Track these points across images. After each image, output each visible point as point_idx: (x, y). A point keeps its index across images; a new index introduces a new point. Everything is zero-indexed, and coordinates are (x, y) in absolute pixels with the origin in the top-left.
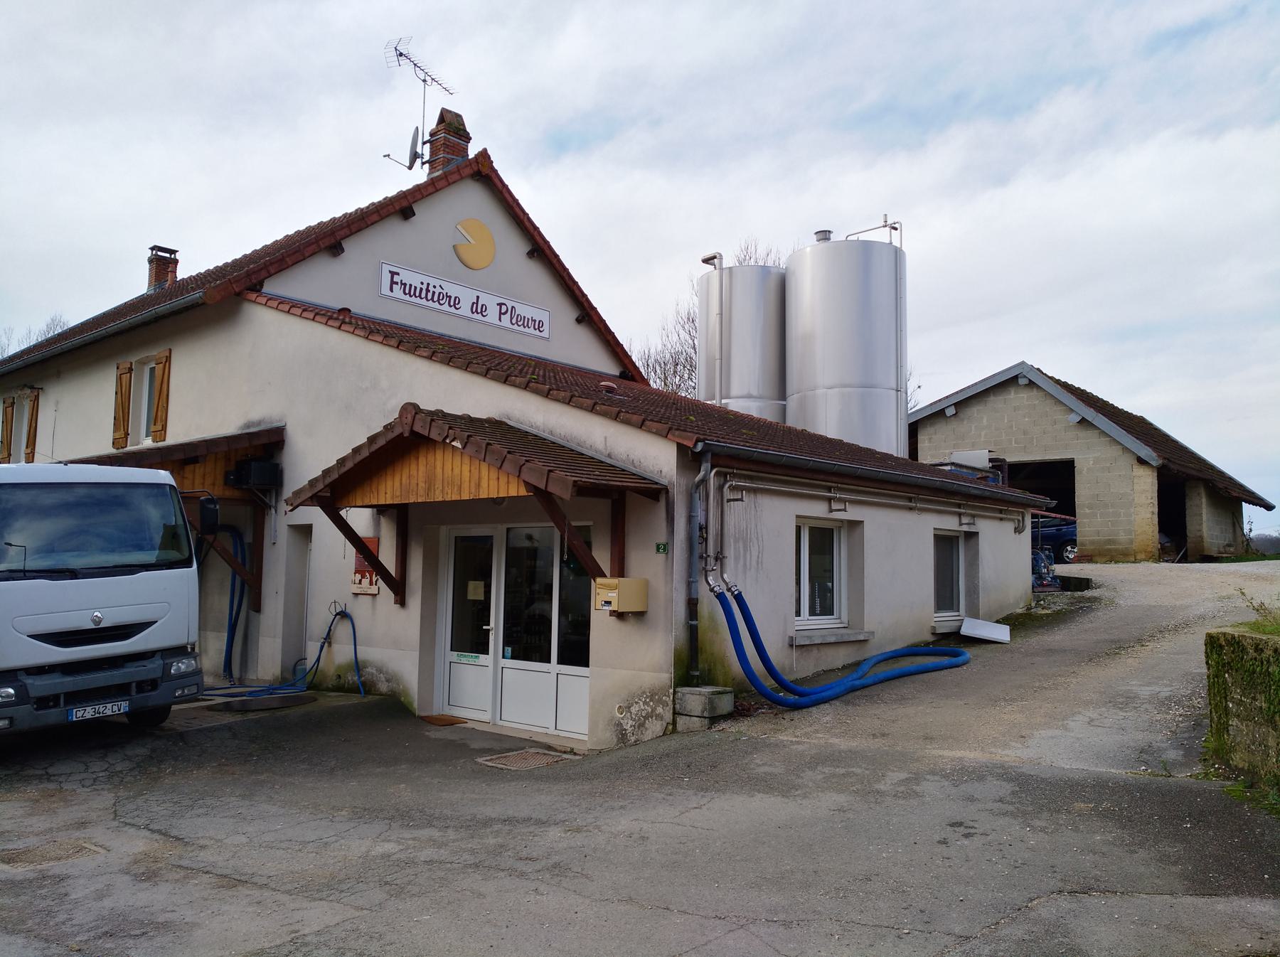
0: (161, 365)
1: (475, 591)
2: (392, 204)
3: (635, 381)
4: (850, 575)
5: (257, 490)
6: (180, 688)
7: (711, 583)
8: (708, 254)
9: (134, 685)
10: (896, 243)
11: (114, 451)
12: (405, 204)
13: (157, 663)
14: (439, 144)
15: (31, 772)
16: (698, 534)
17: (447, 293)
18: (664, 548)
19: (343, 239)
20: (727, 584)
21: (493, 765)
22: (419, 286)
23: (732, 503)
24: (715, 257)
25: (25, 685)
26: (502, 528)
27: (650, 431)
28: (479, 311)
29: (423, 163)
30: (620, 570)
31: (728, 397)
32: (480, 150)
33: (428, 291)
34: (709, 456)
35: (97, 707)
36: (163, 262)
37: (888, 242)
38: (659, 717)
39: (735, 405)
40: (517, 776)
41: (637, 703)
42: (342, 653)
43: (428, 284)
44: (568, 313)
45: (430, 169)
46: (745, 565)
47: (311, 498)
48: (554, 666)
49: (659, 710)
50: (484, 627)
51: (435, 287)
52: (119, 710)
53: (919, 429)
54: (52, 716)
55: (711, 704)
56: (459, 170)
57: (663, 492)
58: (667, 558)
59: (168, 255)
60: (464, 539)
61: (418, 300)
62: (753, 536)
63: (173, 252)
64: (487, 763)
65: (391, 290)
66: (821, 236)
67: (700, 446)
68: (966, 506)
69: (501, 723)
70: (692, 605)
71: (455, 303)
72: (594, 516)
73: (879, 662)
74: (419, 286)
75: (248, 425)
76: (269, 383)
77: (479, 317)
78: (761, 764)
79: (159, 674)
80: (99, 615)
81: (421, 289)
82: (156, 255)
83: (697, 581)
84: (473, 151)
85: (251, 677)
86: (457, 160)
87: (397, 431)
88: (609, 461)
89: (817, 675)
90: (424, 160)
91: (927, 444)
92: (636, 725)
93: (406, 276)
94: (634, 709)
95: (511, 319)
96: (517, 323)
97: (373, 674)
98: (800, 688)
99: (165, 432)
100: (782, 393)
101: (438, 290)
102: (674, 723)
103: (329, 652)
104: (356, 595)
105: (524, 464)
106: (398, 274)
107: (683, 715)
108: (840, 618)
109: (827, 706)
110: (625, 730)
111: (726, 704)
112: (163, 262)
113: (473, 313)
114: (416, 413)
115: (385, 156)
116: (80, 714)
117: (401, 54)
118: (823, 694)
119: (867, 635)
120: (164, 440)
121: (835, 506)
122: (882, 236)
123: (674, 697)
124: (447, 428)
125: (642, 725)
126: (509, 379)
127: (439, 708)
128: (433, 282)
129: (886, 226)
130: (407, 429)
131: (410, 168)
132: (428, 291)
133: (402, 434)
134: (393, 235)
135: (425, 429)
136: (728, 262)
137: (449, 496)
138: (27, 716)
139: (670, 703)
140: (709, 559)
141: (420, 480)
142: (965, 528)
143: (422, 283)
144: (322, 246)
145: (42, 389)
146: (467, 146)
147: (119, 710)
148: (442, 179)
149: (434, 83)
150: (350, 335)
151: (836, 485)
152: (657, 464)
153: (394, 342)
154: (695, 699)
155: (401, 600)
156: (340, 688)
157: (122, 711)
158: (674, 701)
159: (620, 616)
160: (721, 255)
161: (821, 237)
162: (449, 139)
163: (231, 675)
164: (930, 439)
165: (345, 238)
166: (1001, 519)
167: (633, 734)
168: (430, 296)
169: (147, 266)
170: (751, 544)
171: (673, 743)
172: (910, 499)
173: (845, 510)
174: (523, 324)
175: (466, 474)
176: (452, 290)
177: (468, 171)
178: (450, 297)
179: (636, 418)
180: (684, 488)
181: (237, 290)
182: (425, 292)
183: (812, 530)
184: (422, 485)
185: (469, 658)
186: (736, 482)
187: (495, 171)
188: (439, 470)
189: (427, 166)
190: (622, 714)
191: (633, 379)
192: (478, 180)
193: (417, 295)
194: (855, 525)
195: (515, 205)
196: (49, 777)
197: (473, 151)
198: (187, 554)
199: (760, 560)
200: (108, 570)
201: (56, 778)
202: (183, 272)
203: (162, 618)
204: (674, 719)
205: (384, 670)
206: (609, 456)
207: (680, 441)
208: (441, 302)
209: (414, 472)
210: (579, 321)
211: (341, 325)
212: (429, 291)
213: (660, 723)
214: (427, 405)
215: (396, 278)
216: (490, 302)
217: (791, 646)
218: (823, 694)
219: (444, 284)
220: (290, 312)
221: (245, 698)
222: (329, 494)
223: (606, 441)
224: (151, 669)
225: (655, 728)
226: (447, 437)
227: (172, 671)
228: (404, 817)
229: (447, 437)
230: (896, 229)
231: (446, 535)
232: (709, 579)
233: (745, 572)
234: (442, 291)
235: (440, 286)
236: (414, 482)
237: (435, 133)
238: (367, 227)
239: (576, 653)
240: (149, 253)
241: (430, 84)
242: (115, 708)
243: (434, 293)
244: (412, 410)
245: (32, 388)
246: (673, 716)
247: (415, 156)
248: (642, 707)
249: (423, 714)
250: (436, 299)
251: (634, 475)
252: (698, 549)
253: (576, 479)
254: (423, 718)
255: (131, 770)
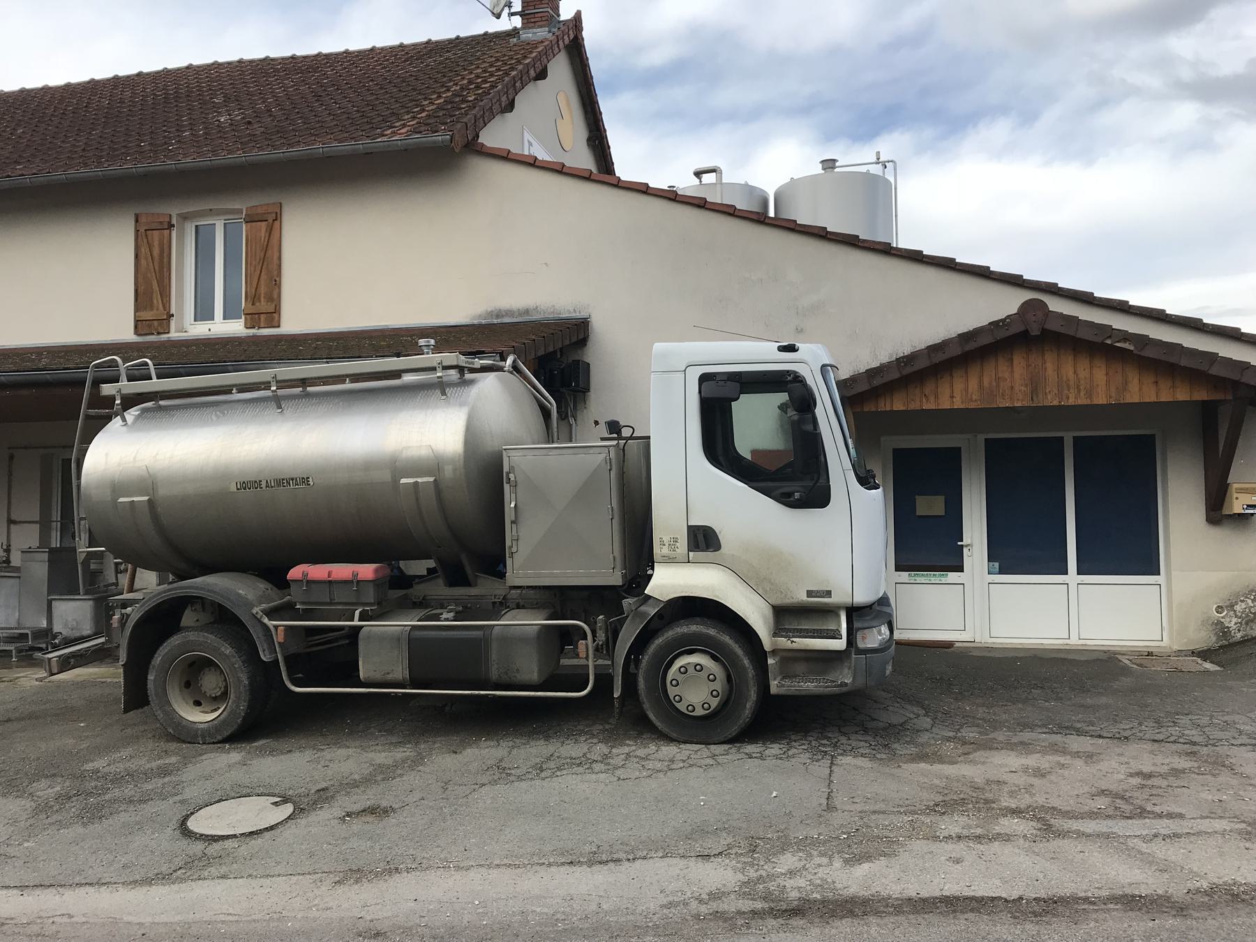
50: (959, 543)
75: (490, 314)
76: (546, 264)
90: (512, 11)
92: (1243, 622)
120: (279, 326)
129: (879, 163)
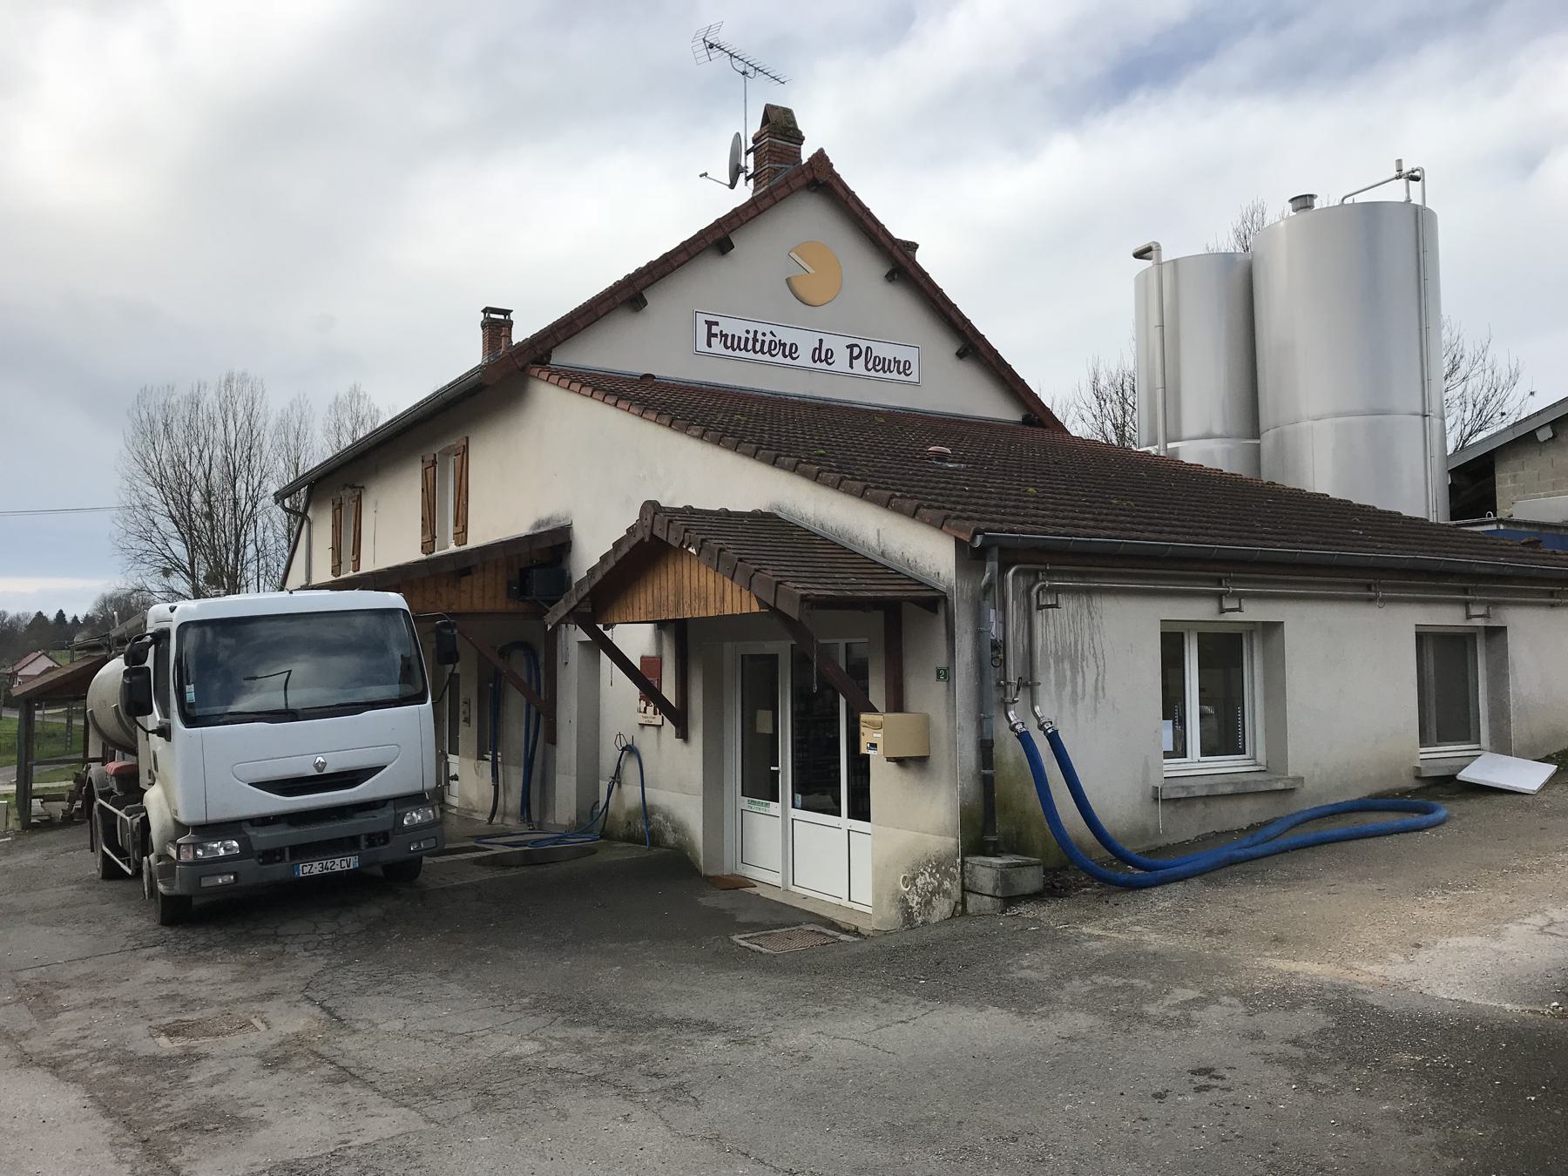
0: (459, 456)
1: (764, 725)
2: (704, 238)
3: (1044, 426)
4: (1267, 697)
5: (543, 601)
6: (414, 842)
7: (1012, 719)
8: (1141, 245)
9: (363, 838)
10: (1416, 200)
11: (424, 557)
12: (719, 235)
13: (387, 814)
14: (763, 151)
15: (260, 931)
16: (992, 654)
17: (780, 341)
18: (945, 674)
19: (644, 288)
20: (1038, 719)
21: (747, 945)
22: (744, 335)
23: (1050, 610)
24: (1149, 249)
25: (249, 838)
26: (842, 643)
27: (923, 521)
28: (823, 358)
29: (747, 179)
30: (897, 703)
31: (1179, 439)
32: (815, 151)
33: (755, 340)
34: (996, 550)
35: (324, 862)
36: (496, 325)
37: (1403, 200)
38: (947, 894)
39: (1190, 453)
40: (771, 965)
41: (922, 874)
42: (630, 795)
43: (756, 332)
44: (942, 347)
45: (755, 186)
46: (1074, 692)
47: (567, 614)
48: (844, 821)
49: (947, 884)
51: (764, 334)
52: (349, 866)
53: (1496, 464)
54: (278, 871)
55: (1004, 877)
56: (787, 183)
57: (942, 601)
58: (948, 686)
59: (502, 317)
60: (753, 657)
61: (743, 354)
62: (1087, 653)
63: (507, 312)
64: (741, 941)
65: (709, 345)
66: (1299, 203)
67: (979, 540)
68: (1477, 591)
69: (793, 889)
70: (986, 749)
71: (791, 351)
72: (863, 637)
73: (1297, 824)
74: (744, 335)
75: (538, 524)
77: (824, 365)
78: (1031, 967)
79: (389, 826)
80: (322, 760)
81: (747, 339)
82: (489, 318)
83: (991, 718)
84: (806, 153)
85: (549, 822)
86: (787, 169)
87: (639, 536)
88: (882, 561)
89: (1204, 839)
90: (748, 174)
91: (1510, 484)
93: (727, 326)
94: (919, 882)
95: (867, 363)
96: (874, 367)
97: (660, 822)
98: (1146, 860)
99: (466, 533)
100: (1255, 430)
101: (768, 338)
102: (964, 902)
103: (619, 793)
104: (642, 725)
105: (754, 574)
106: (716, 324)
107: (973, 892)
108: (1254, 758)
109: (1180, 885)
110: (912, 908)
111: (1031, 880)
112: (496, 325)
113: (815, 362)
114: (655, 513)
115: (701, 176)
116: (306, 870)
117: (711, 46)
118: (1177, 869)
119: (1291, 782)
120: (466, 543)
121: (1228, 604)
122: (1395, 192)
123: (962, 869)
124: (683, 530)
125: (928, 903)
126: (778, 460)
127: (729, 867)
128: (761, 328)
130: (647, 532)
131: (732, 186)
132: (755, 340)
133: (643, 539)
134: (712, 275)
135: (663, 532)
136: (1166, 256)
137: (696, 612)
138: (255, 873)
139: (958, 876)
140: (1009, 687)
141: (670, 594)
142: (1479, 622)
143: (748, 332)
144: (619, 301)
145: (363, 487)
146: (800, 149)
147: (349, 866)
148: (766, 196)
149: (758, 73)
150: (625, 413)
151: (1228, 575)
152: (934, 564)
153: (666, 420)
154: (986, 870)
155: (683, 734)
156: (631, 838)
157: (351, 867)
158: (962, 873)
159: (901, 762)
160: (1158, 245)
161: (1299, 206)
162: (775, 143)
163: (529, 818)
164: (1515, 476)
165: (647, 287)
166: (1552, 606)
167: (920, 913)
168: (758, 347)
169: (481, 331)
170: (1084, 664)
171: (960, 926)
172: (1369, 587)
173: (1239, 610)
174: (883, 368)
175: (711, 584)
176: (786, 336)
177: (801, 181)
178: (785, 345)
179: (909, 504)
180: (970, 594)
181: (520, 364)
182: (753, 343)
183: (1203, 640)
184: (671, 598)
185: (759, 805)
186: (1050, 581)
187: (837, 177)
188: (686, 582)
189: (751, 181)
190: (907, 887)
191: (1041, 424)
192: (815, 191)
193: (742, 347)
194: (1272, 629)
195: (864, 217)
196: (275, 939)
197: (806, 153)
198: (420, 688)
199: (1100, 685)
200: (332, 709)
201: (283, 938)
202: (520, 334)
203: (391, 763)
204: (963, 897)
205: (671, 817)
206: (883, 554)
207: (956, 534)
208: (773, 352)
209: (664, 583)
210: (960, 355)
211: (617, 401)
212: (757, 341)
213: (947, 901)
214: (672, 498)
215: (715, 330)
216: (838, 345)
217: (1156, 799)
218: (1177, 869)
219: (775, 329)
220: (571, 388)
221: (527, 848)
222: (590, 610)
223: (879, 535)
224: (384, 816)
225: (942, 907)
226: (683, 542)
227: (405, 822)
228: (578, 1010)
229: (683, 542)
230: (1417, 179)
231: (731, 653)
232: (1010, 714)
233: (1074, 702)
234: (773, 338)
235: (771, 332)
236: (664, 594)
237: (757, 139)
238: (673, 270)
239: (860, 811)
240: (481, 317)
241: (752, 76)
242: (344, 864)
243: (763, 342)
244: (652, 509)
245: (353, 487)
246: (963, 894)
247: (736, 171)
248: (928, 880)
249: (711, 873)
250: (766, 349)
251: (910, 578)
252: (993, 675)
253: (804, 592)
254: (707, 878)
255: (359, 933)
